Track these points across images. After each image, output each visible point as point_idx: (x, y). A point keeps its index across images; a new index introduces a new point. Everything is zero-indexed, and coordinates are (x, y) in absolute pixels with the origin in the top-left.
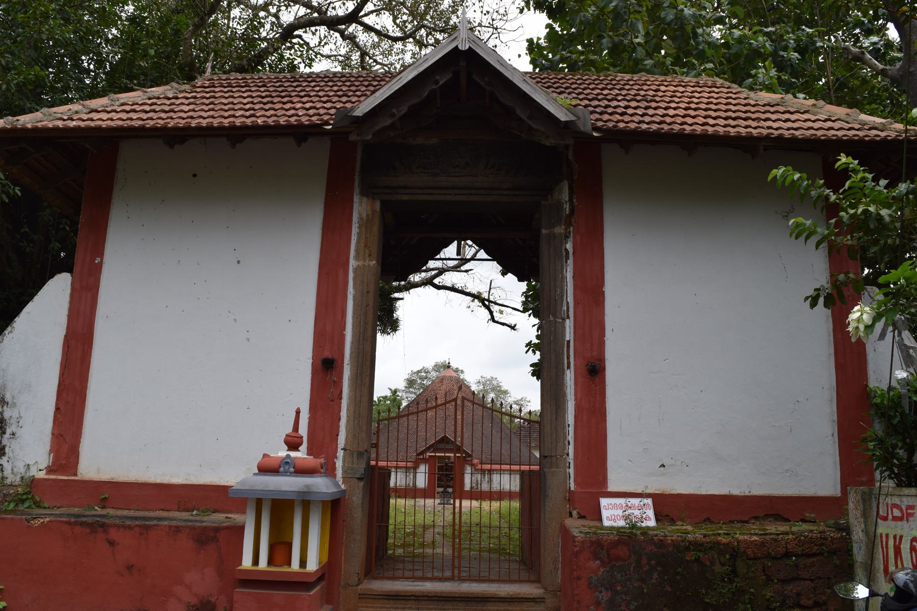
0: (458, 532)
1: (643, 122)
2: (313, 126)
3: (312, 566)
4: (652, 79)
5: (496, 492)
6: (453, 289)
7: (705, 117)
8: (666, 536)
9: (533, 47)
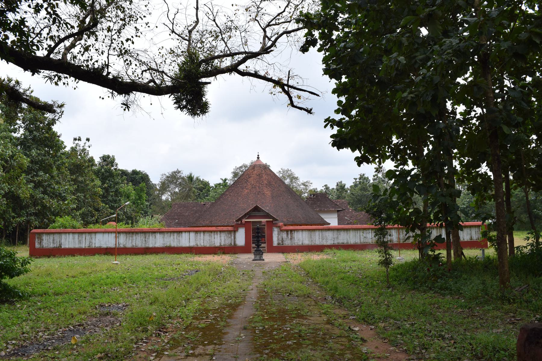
6: (256, 75)
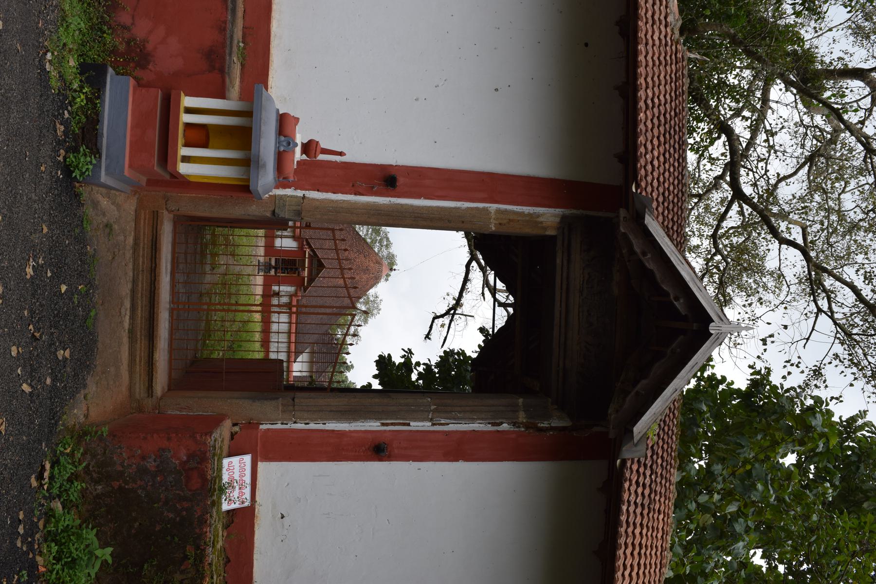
2: (635, 172)
3: (184, 169)
4: (670, 504)
5: (269, 317)
6: (466, 280)
8: (210, 526)
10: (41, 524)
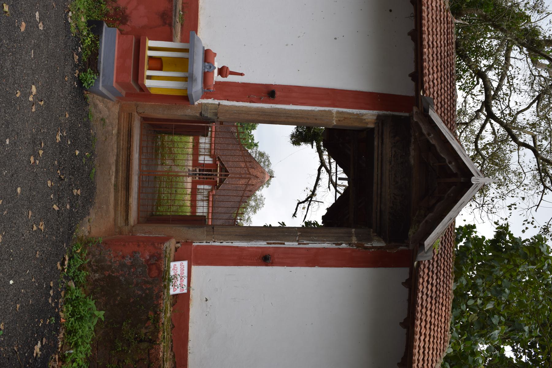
0: (172, 179)
1: (423, 295)
2: (422, 84)
3: (148, 83)
4: (450, 302)
5: (195, 204)
6: (318, 179)
7: (425, 334)
8: (163, 300)
9: (470, 228)
10: (62, 294)
